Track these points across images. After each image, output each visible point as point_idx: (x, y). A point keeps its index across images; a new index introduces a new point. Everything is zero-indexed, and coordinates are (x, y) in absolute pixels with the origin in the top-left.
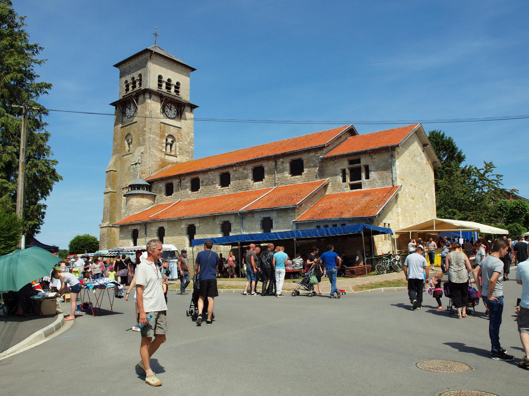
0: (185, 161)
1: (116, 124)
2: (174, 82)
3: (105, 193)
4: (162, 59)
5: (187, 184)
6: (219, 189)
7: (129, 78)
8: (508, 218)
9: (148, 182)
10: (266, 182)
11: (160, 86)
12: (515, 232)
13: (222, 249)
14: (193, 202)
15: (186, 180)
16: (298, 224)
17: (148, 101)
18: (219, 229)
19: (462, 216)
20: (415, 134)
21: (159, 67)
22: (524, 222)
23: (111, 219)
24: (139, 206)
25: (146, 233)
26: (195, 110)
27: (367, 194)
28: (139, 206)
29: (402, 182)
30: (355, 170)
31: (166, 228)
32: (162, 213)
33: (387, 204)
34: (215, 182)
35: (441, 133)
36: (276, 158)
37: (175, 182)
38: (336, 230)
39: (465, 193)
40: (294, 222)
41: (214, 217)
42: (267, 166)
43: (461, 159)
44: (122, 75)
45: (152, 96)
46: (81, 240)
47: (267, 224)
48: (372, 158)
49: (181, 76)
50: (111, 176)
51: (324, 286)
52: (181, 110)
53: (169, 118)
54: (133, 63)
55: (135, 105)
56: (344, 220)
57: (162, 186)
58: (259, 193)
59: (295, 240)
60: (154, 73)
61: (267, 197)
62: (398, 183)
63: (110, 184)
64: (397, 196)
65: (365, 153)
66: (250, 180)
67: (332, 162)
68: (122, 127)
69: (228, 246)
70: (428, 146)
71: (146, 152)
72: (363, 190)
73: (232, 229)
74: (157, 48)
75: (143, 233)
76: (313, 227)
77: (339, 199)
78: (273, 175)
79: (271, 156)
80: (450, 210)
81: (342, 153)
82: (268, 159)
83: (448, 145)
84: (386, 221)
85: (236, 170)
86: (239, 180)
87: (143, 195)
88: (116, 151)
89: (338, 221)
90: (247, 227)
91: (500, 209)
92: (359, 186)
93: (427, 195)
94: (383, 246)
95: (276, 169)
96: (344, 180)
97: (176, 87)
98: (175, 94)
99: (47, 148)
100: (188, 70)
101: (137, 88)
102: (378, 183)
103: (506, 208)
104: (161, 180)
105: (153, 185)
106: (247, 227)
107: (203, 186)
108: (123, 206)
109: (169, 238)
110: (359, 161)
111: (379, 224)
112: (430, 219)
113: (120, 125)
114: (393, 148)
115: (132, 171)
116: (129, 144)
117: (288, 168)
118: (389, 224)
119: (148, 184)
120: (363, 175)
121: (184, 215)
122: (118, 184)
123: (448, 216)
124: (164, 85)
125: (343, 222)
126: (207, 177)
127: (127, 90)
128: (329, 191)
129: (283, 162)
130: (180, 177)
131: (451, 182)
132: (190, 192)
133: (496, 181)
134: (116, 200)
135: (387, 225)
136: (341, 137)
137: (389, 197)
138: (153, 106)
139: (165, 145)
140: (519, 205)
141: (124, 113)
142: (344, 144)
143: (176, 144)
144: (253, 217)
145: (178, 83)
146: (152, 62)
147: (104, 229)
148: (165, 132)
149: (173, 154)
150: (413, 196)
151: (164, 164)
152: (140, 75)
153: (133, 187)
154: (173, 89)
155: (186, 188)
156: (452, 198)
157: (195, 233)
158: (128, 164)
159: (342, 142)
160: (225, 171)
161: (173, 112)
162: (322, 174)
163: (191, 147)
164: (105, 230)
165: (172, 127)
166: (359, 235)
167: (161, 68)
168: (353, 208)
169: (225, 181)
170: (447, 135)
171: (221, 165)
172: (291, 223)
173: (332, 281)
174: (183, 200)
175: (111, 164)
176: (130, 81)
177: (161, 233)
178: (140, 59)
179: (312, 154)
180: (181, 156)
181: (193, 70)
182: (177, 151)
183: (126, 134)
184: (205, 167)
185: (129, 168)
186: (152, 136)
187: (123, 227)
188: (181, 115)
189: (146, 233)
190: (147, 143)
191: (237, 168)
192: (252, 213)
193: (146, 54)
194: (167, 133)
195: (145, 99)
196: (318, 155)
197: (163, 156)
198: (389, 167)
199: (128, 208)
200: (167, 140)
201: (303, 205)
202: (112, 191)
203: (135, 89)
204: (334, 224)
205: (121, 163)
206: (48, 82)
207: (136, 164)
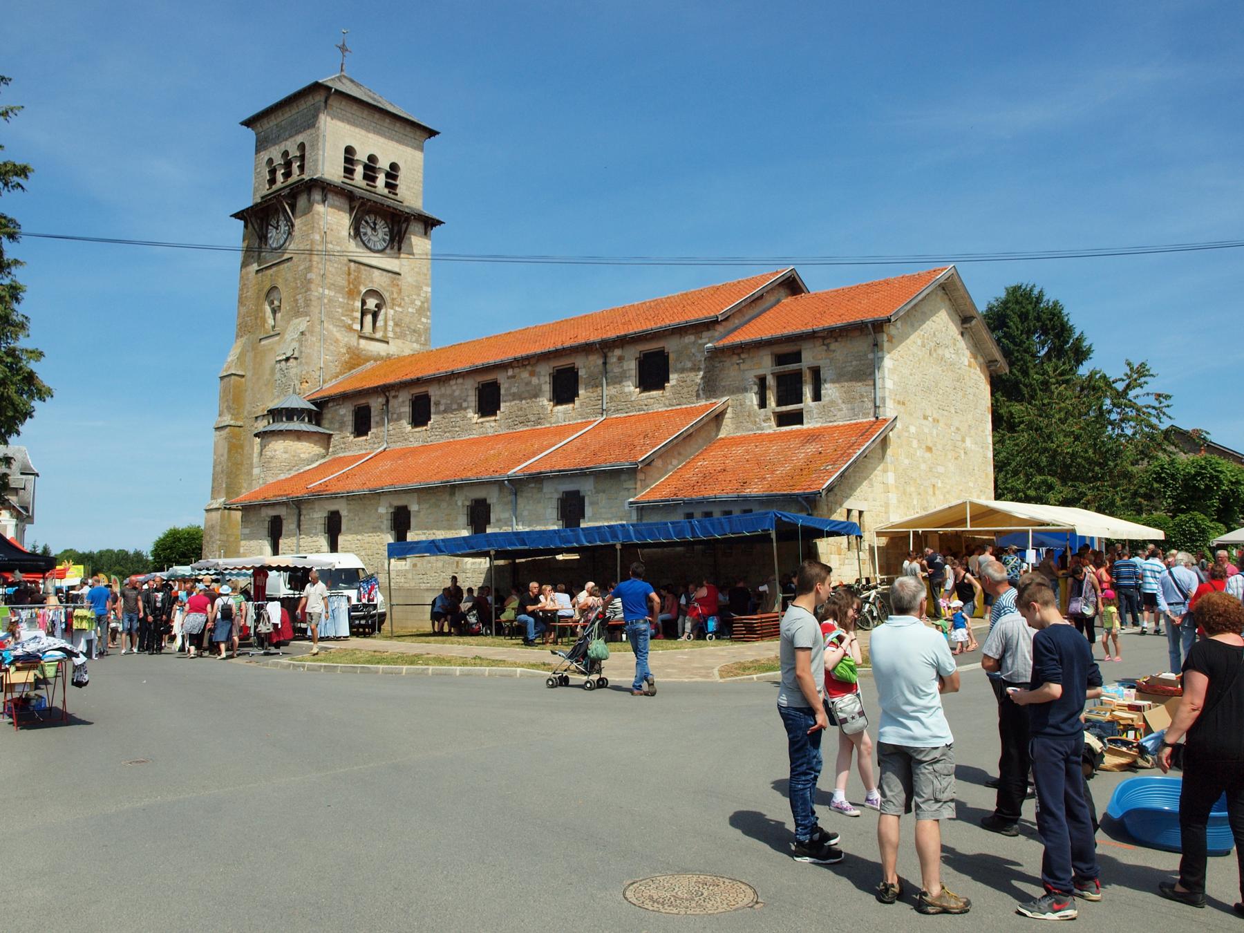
0: (407, 352)
1: (245, 264)
2: (384, 164)
3: (217, 429)
4: (355, 108)
5: (403, 410)
6: (474, 421)
7: (275, 153)
8: (1178, 500)
9: (314, 402)
10: (581, 405)
11: (349, 172)
12: (1193, 534)
13: (469, 566)
14: (413, 451)
15: (400, 400)
16: (642, 509)
17: (319, 208)
18: (463, 519)
19: (1067, 492)
20: (941, 293)
21: (348, 127)
22: (1218, 511)
23: (231, 490)
24: (290, 461)
25: (299, 526)
26: (436, 229)
27: (813, 436)
28: (290, 461)
29: (901, 408)
30: (790, 379)
31: (344, 513)
32: (338, 479)
33: (855, 462)
34: (465, 405)
35: (1036, 292)
36: (605, 347)
37: (376, 404)
38: (713, 525)
39: (1077, 438)
40: (631, 503)
41: (451, 489)
42: (586, 366)
43: (1081, 354)
44: (261, 145)
45: (330, 196)
46: (179, 540)
47: (572, 508)
48: (828, 349)
49: (402, 148)
50: (233, 389)
51: (618, 662)
52: (399, 231)
53: (370, 249)
54: (286, 116)
55: (288, 220)
56: (746, 499)
57: (346, 412)
58: (560, 433)
59: (618, 547)
60: (334, 142)
61: (578, 443)
62: (889, 411)
63: (229, 408)
64: (884, 442)
65: (812, 336)
66: (545, 402)
67: (735, 359)
68: (257, 271)
69: (482, 560)
70: (974, 322)
71: (312, 332)
72: (805, 426)
73: (493, 517)
74: (344, 81)
75: (293, 526)
76: (678, 517)
77: (747, 449)
78: (599, 389)
79: (593, 344)
80: (1039, 478)
81: (758, 337)
82: (586, 349)
83: (1051, 320)
84: (853, 503)
85: (513, 377)
86: (521, 399)
87: (299, 435)
88: (243, 329)
89: (733, 502)
90: (525, 513)
91: (1159, 479)
92: (797, 418)
93: (968, 440)
94: (843, 563)
95: (605, 375)
96: (763, 404)
97: (388, 175)
98: (386, 191)
99: (21, 319)
100: (418, 133)
101: (295, 177)
102: (840, 410)
103: (1173, 477)
104: (344, 397)
105: (325, 411)
106: (525, 513)
107: (438, 413)
108: (255, 460)
109: (350, 537)
110: (797, 357)
111: (831, 511)
112: (959, 502)
113: (255, 267)
114: (879, 326)
115: (278, 376)
116: (274, 312)
117: (633, 373)
118: (861, 513)
119: (313, 407)
120: (808, 392)
121: (386, 483)
122: (248, 407)
123: (1032, 493)
124: (359, 170)
125: (746, 504)
126: (449, 391)
127: (272, 181)
128: (727, 429)
129: (620, 359)
130: (385, 390)
131: (1043, 411)
132: (409, 428)
133: (1154, 408)
134: (242, 447)
135: (855, 514)
136: (761, 297)
137: (861, 445)
138: (331, 221)
139: (358, 315)
140: (1205, 468)
141: (263, 238)
142: (770, 314)
143: (387, 313)
144: (540, 490)
145: (394, 166)
146: (328, 114)
147: (214, 514)
148: (359, 283)
149: (379, 335)
150: (930, 445)
151: (355, 359)
152: (302, 147)
153: (276, 414)
154: (381, 180)
155: (399, 419)
156: (1046, 450)
157: (409, 528)
158: (270, 361)
159: (764, 311)
160: (489, 378)
161: (380, 235)
162: (710, 387)
163: (424, 320)
164: (216, 516)
165: (377, 273)
166: (765, 538)
167: (353, 128)
168: (773, 472)
169: (488, 403)
170: (1050, 296)
171: (479, 362)
172: (627, 507)
173: (639, 651)
174: (393, 446)
175: (231, 358)
176: (279, 160)
177: (333, 529)
178: (301, 108)
179: (689, 339)
180: (399, 342)
181: (432, 133)
182: (390, 329)
183: (266, 290)
184: (445, 368)
185: (273, 370)
186: (328, 291)
187: (248, 509)
188: (400, 242)
189: (299, 526)
190: (315, 310)
191: (517, 370)
192: (537, 479)
193: (317, 96)
194: (365, 286)
195: (309, 209)
196: (704, 341)
197: (353, 340)
198: (869, 371)
199: (266, 465)
200: (364, 303)
201: (658, 463)
202: (232, 423)
203: (290, 180)
204: (726, 509)
205: (255, 357)
206: (20, 162)
207: (287, 359)
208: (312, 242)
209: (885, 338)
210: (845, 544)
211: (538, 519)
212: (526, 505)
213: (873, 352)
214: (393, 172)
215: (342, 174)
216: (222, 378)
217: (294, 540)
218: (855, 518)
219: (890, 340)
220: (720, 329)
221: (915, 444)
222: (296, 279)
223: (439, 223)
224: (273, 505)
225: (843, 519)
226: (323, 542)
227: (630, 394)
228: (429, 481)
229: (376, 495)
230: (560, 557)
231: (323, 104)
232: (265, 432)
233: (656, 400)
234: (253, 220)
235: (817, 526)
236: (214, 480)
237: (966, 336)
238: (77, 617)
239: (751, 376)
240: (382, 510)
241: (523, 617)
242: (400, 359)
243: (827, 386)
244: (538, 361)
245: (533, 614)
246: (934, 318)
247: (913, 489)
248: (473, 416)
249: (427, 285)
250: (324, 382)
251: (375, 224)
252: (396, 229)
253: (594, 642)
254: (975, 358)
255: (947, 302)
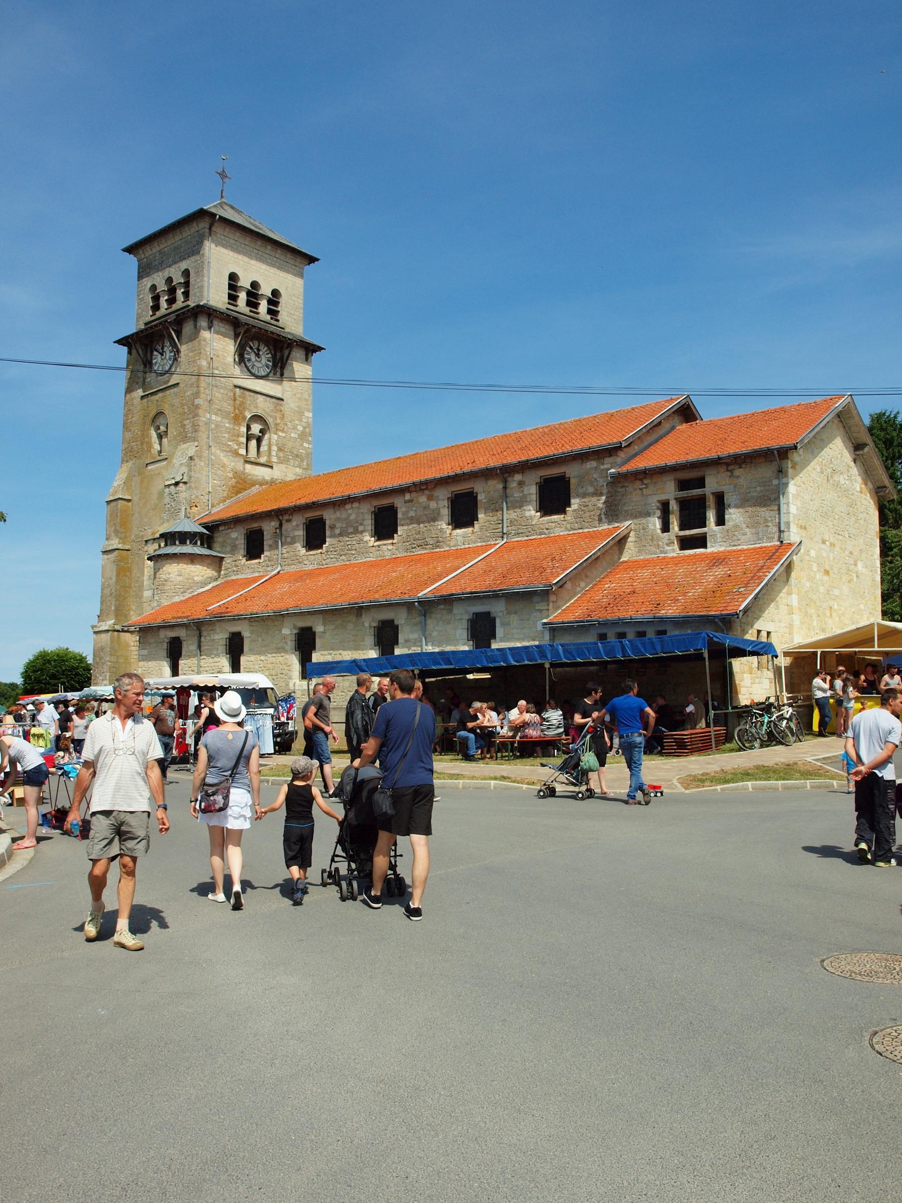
0: (290, 477)
1: (129, 390)
2: (266, 290)
3: (105, 552)
6: (371, 544)
7: (159, 279)
10: (481, 529)
11: (233, 298)
14: (310, 574)
15: (294, 523)
16: (554, 629)
17: (205, 334)
18: (370, 640)
20: (836, 421)
21: (231, 253)
23: (120, 612)
24: (185, 583)
25: (199, 647)
26: (316, 356)
27: (718, 560)
28: (185, 583)
30: (693, 504)
31: (246, 634)
33: (766, 584)
34: (361, 528)
36: (505, 472)
37: (269, 527)
38: (643, 644)
40: (545, 624)
41: (358, 610)
42: (484, 491)
44: (144, 271)
45: (215, 322)
46: (49, 662)
47: (482, 629)
50: (119, 512)
54: (169, 243)
55: (174, 345)
56: (662, 620)
57: (238, 536)
59: (547, 666)
60: (219, 268)
62: (793, 535)
63: (116, 532)
64: (789, 568)
66: (444, 525)
67: (638, 484)
68: (142, 397)
70: (866, 450)
72: (709, 550)
74: (226, 207)
75: (194, 647)
76: (590, 638)
77: (650, 572)
78: (499, 514)
79: (495, 469)
81: (662, 463)
82: (487, 474)
84: (763, 624)
87: (192, 558)
90: (435, 634)
92: (701, 542)
93: (860, 564)
94: (753, 683)
96: (666, 528)
98: (268, 317)
100: (299, 260)
101: (180, 303)
102: (745, 534)
104: (236, 521)
107: (332, 536)
108: (146, 582)
109: (253, 658)
111: (744, 632)
112: (867, 623)
113: (140, 392)
114: (784, 453)
115: (167, 500)
116: (160, 437)
117: (534, 497)
118: (769, 633)
120: (711, 516)
121: (290, 604)
124: (243, 296)
125: (662, 625)
126: (344, 516)
127: (156, 308)
128: (630, 553)
129: (521, 484)
130: (279, 514)
134: (130, 570)
135: (764, 634)
137: (770, 568)
138: (219, 346)
139: (244, 440)
141: (148, 364)
144: (450, 611)
145: (276, 293)
146: (213, 241)
147: (103, 635)
148: (245, 409)
149: (263, 460)
150: (827, 568)
151: (242, 483)
152: (186, 273)
155: (293, 542)
157: (314, 648)
158: (158, 485)
159: (661, 437)
160: (385, 502)
161: (262, 361)
162: (612, 512)
163: (306, 445)
164: (105, 637)
165: (261, 398)
166: (699, 657)
168: (685, 594)
171: (376, 487)
172: (540, 627)
175: (117, 481)
176: (162, 287)
177: (235, 650)
178: (185, 235)
179: (591, 464)
180: (283, 467)
181: (312, 260)
182: (274, 453)
183: (153, 414)
185: (161, 495)
186: (214, 418)
187: (146, 632)
189: (199, 647)
190: (202, 435)
191: (414, 495)
192: (447, 601)
194: (250, 412)
195: (195, 335)
196: (606, 466)
197: (239, 465)
198: (773, 496)
199: (159, 587)
200: (249, 428)
201: (569, 585)
202: (120, 546)
203: (175, 307)
205: (142, 481)
207: (177, 484)
208: (200, 368)
209: (790, 465)
210: (756, 664)
211: (451, 640)
212: (434, 625)
213: (778, 478)
214: (274, 299)
215: (227, 300)
216: (108, 502)
217: (194, 661)
218: (763, 638)
219: (793, 467)
220: (622, 455)
221: (815, 568)
222: (182, 405)
223: (320, 349)
224: (172, 627)
225: (754, 639)
226: (224, 662)
227: (531, 518)
228: (335, 603)
229: (280, 617)
230: (470, 676)
231: (207, 231)
232: (160, 556)
233: (557, 525)
234: (138, 346)
235: (741, 646)
236: (102, 603)
237: (858, 463)
238: (34, 735)
239: (654, 502)
240: (286, 631)
241: (463, 733)
242: (285, 484)
243: (731, 510)
244: (436, 485)
245: (472, 731)
246: (831, 445)
247: (813, 611)
248: (369, 539)
249: (308, 411)
250: (212, 506)
251: (259, 350)
252: (278, 354)
253: (586, 755)
254: (866, 484)
255: (842, 429)
